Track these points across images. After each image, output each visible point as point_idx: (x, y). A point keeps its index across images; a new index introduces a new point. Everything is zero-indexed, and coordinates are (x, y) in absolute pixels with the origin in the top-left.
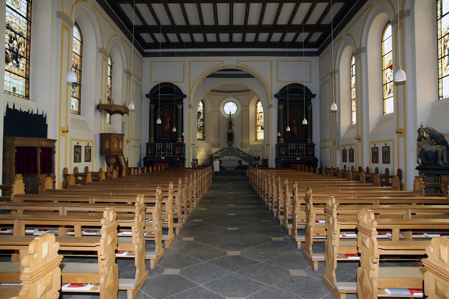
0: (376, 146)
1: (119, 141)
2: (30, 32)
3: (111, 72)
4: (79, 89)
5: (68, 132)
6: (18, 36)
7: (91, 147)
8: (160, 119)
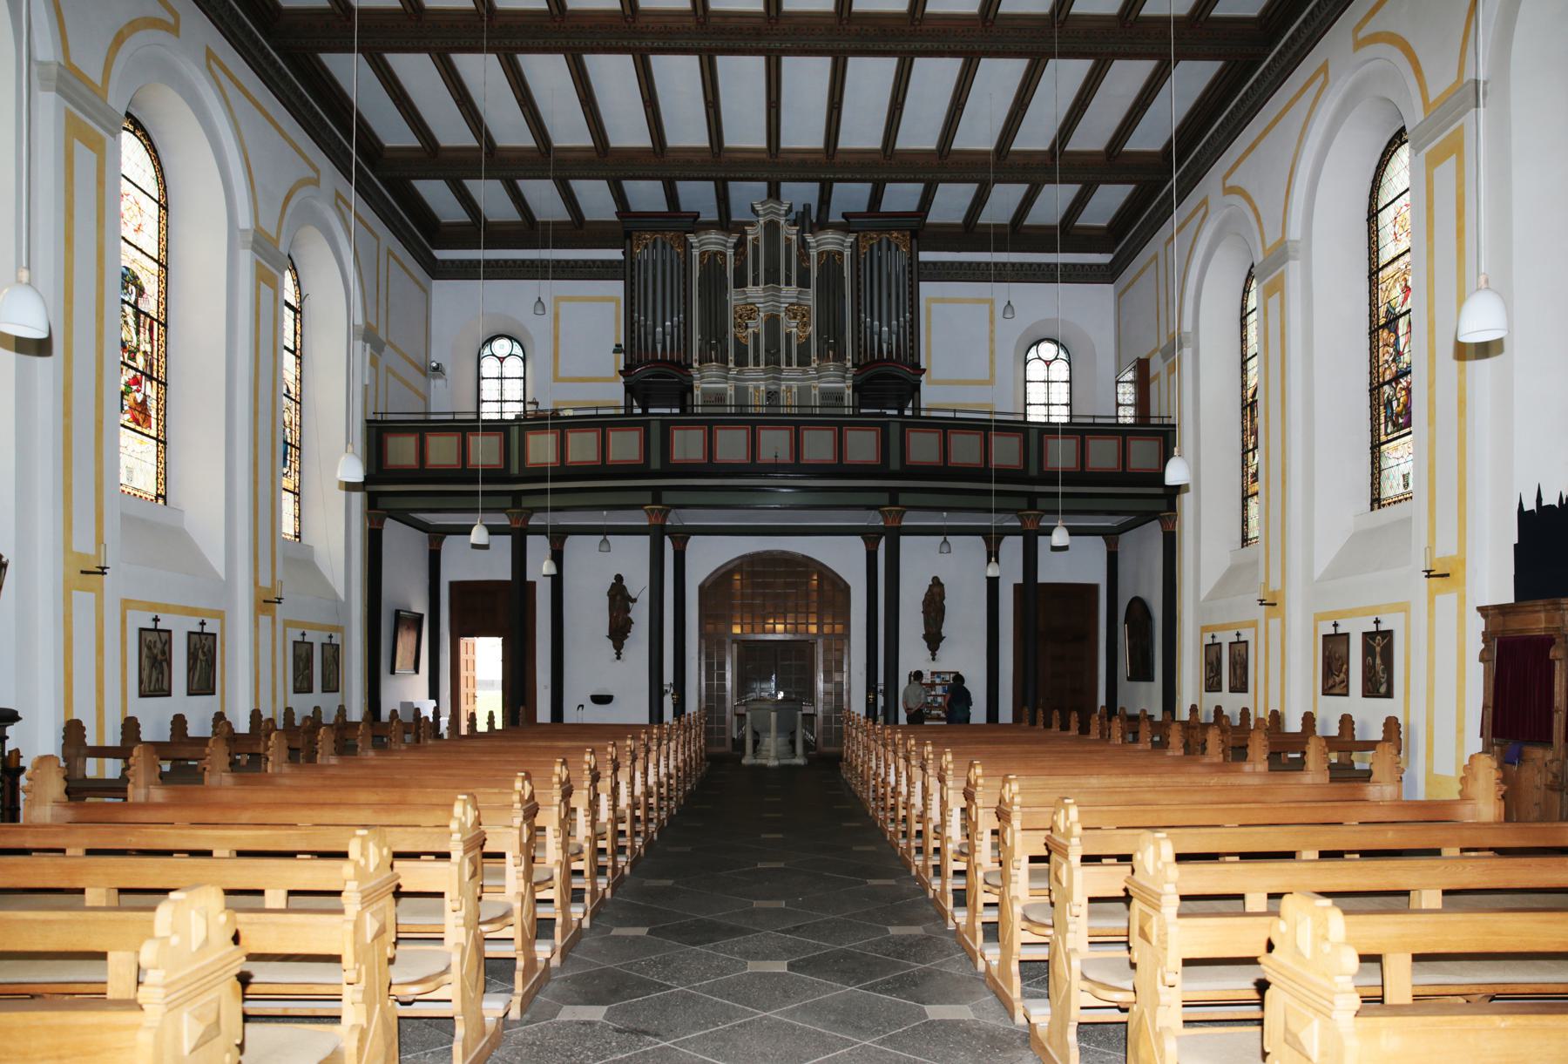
0: (1242, 639)
5: (279, 603)
7: (214, 635)
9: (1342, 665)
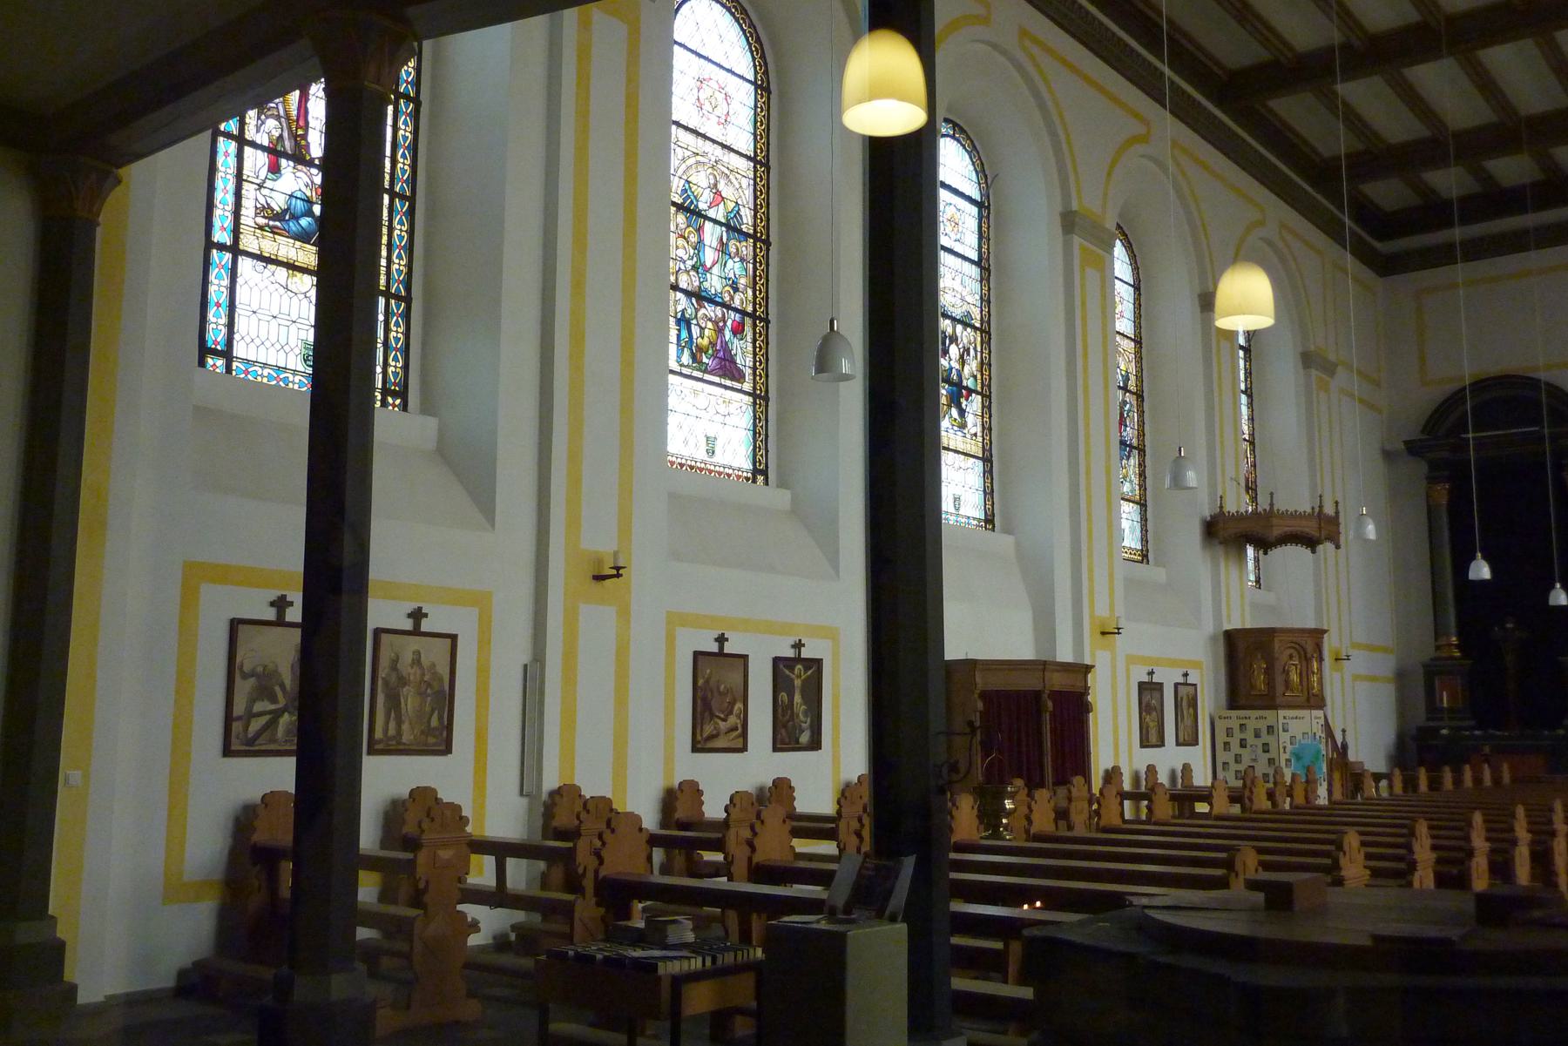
1: (1308, 660)
2: (989, 302)
3: (1248, 374)
4: (1140, 464)
5: (1119, 633)
6: (959, 328)
7: (1195, 685)
8: (1484, 558)
9: (732, 704)
